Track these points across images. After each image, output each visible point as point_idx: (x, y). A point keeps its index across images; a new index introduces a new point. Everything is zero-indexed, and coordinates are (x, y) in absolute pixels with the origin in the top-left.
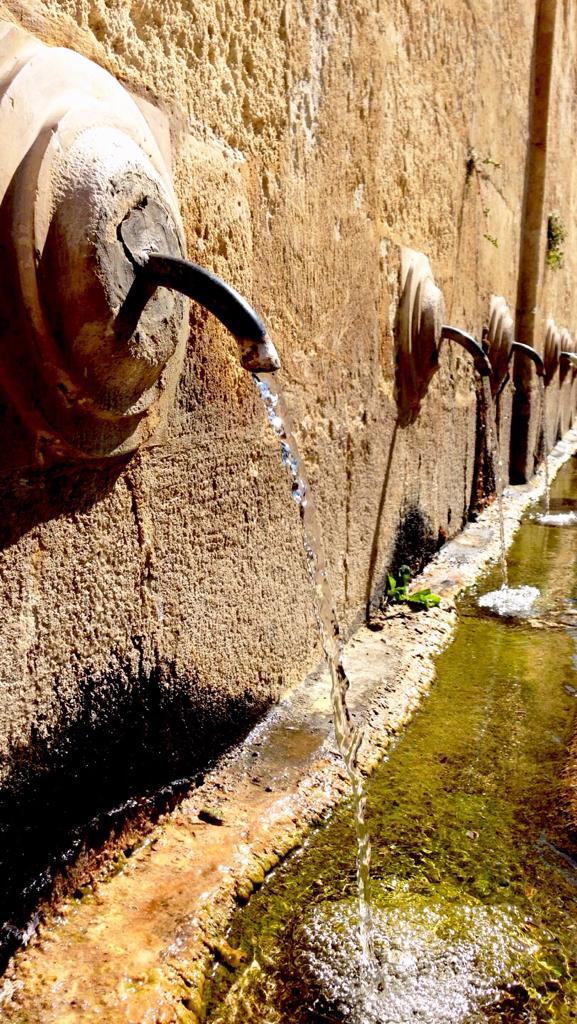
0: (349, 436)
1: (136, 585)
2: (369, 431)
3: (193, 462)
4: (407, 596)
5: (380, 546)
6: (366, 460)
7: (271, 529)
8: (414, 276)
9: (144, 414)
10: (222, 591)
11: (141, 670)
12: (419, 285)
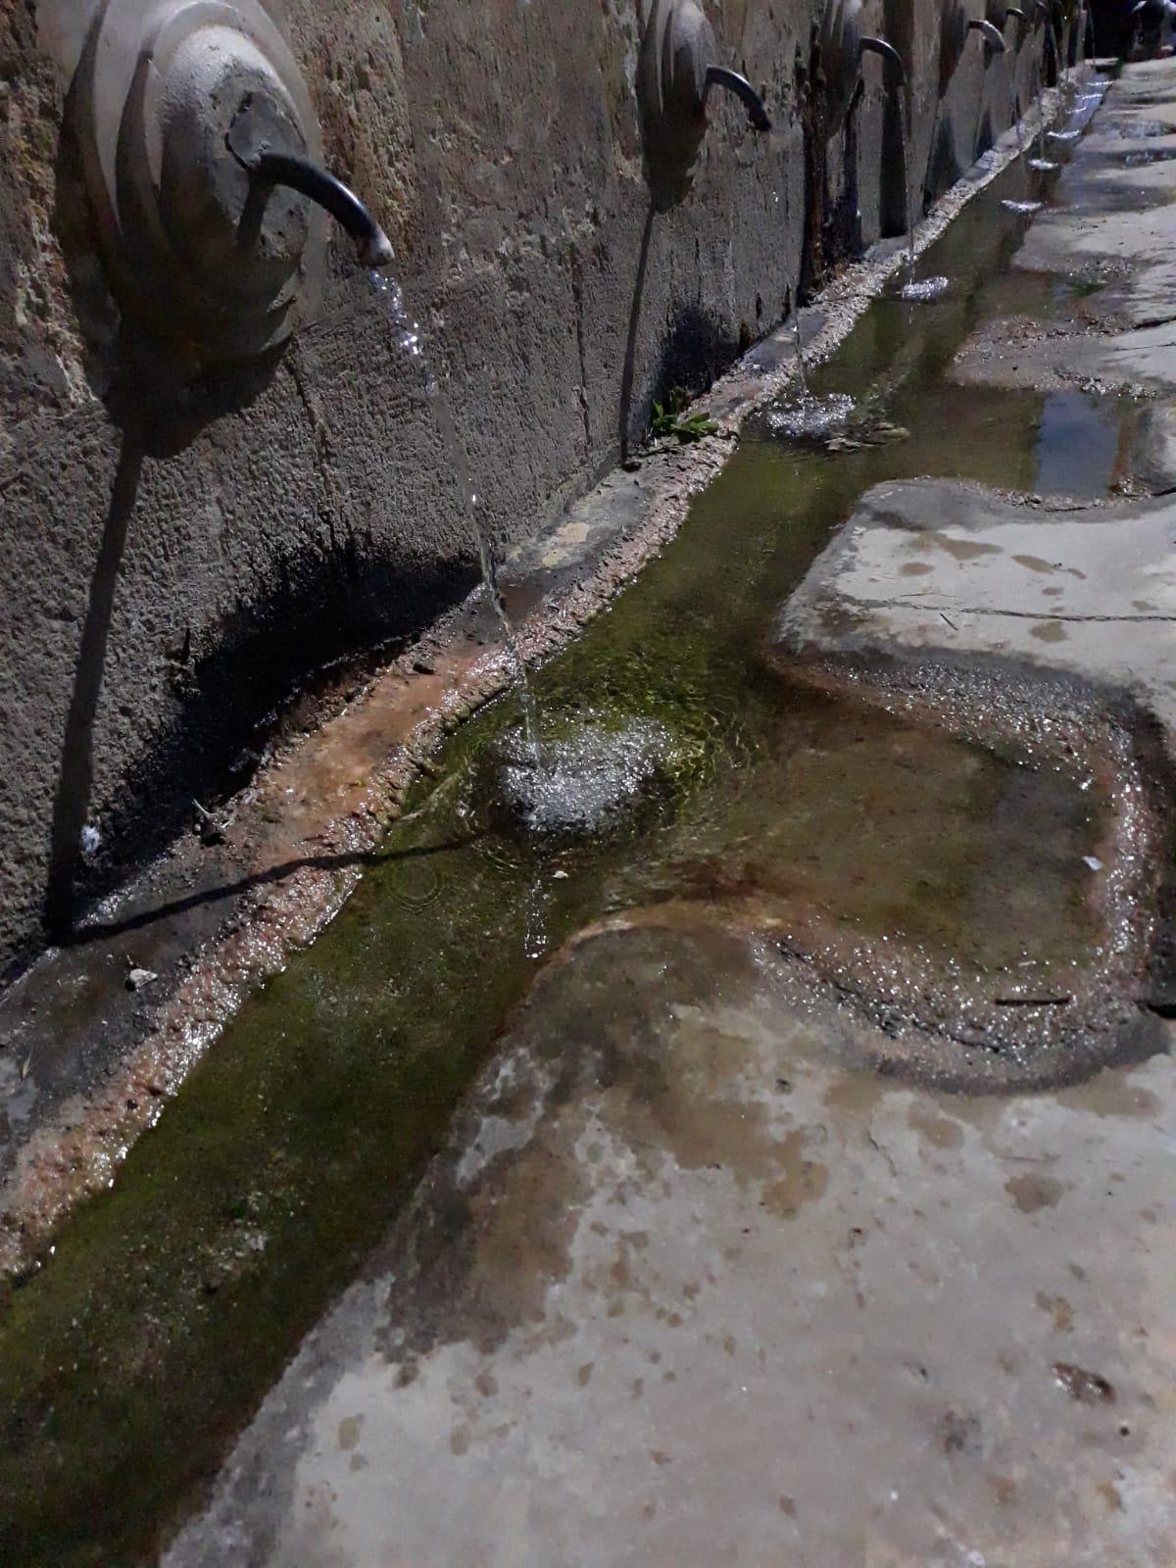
1: (315, 464)
3: (358, 329)
5: (637, 367)
6: (602, 270)
9: (291, 301)
11: (334, 543)
12: (670, 15)
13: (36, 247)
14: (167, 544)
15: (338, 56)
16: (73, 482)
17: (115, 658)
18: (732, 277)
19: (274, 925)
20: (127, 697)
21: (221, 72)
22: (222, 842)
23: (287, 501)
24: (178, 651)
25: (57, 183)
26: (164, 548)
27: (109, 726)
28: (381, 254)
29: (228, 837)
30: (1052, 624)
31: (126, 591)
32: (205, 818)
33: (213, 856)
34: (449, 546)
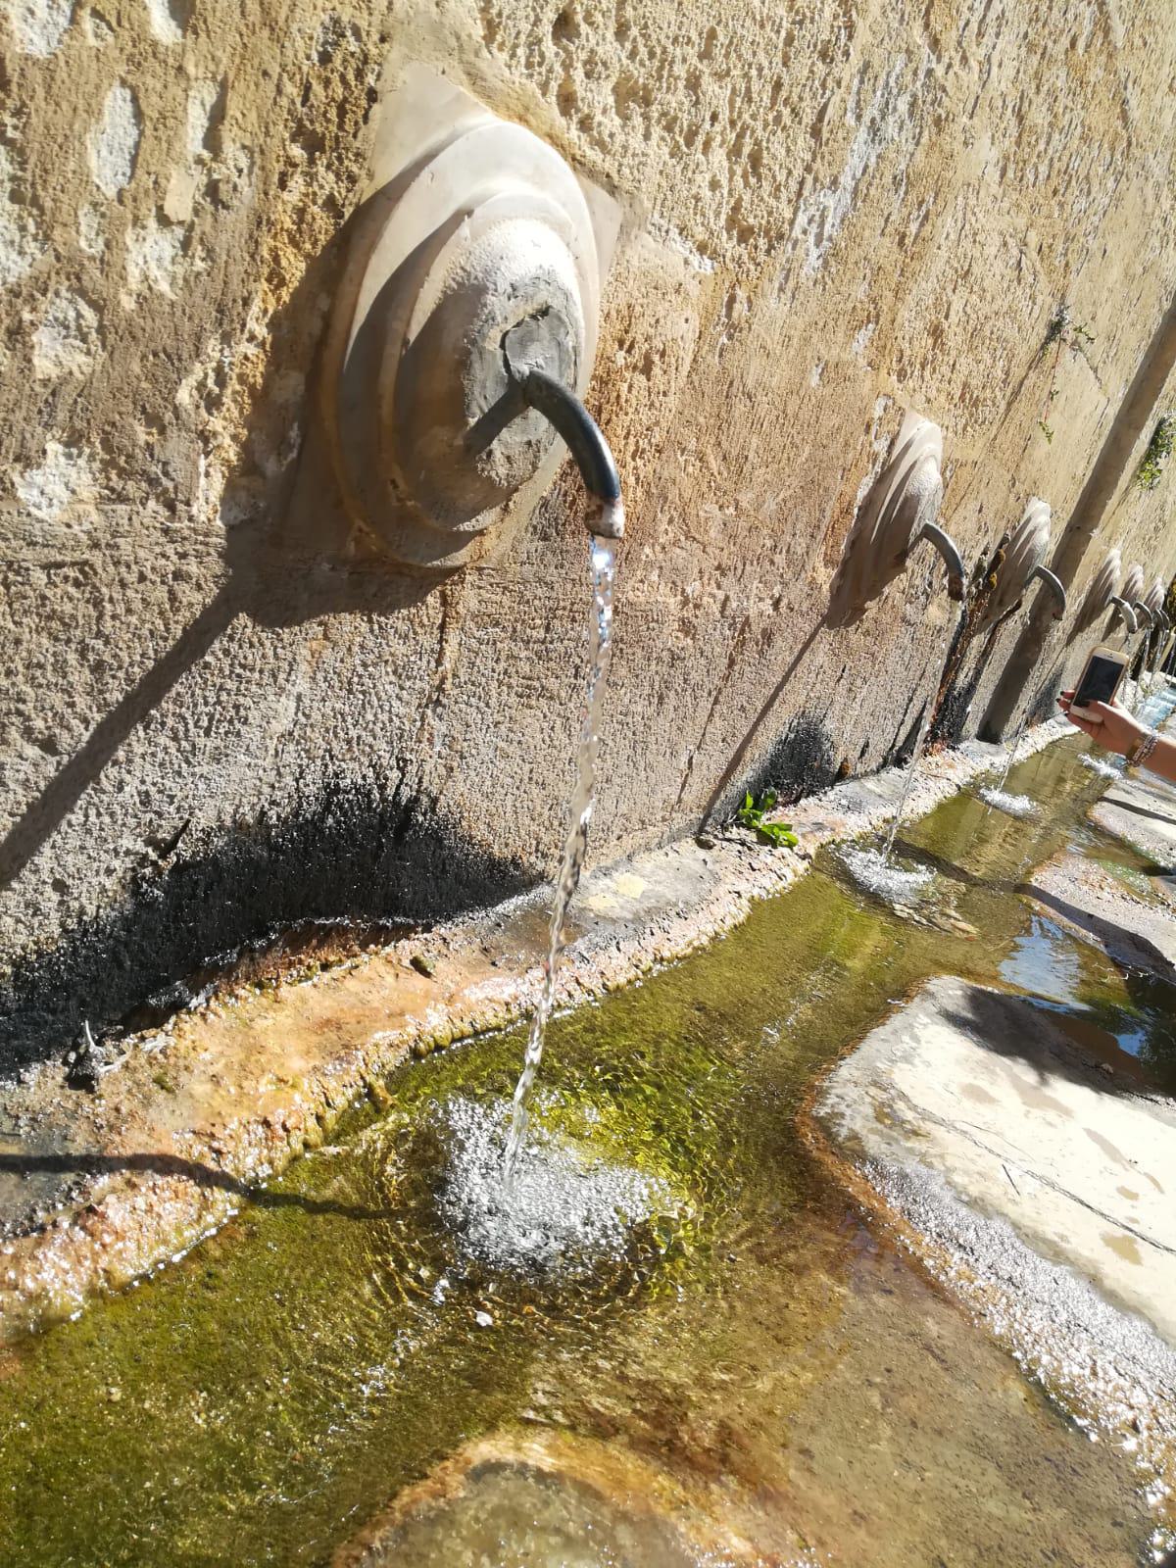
1: (420, 706)
2: (778, 620)
3: (528, 595)
5: (748, 755)
6: (761, 653)
9: (481, 533)
11: (397, 793)
12: (912, 467)
13: (242, 331)
14: (217, 716)
15: (640, 330)
16: (143, 600)
17: (83, 819)
19: (94, 1241)
20: (72, 870)
21: (533, 270)
22: (91, 1090)
23: (372, 731)
24: (164, 840)
25: (303, 281)
26: (210, 721)
27: (28, 896)
28: (612, 525)
29: (102, 1087)
30: (1125, 1237)
31: (139, 749)
32: (87, 1051)
33: (70, 1105)
34: (507, 845)
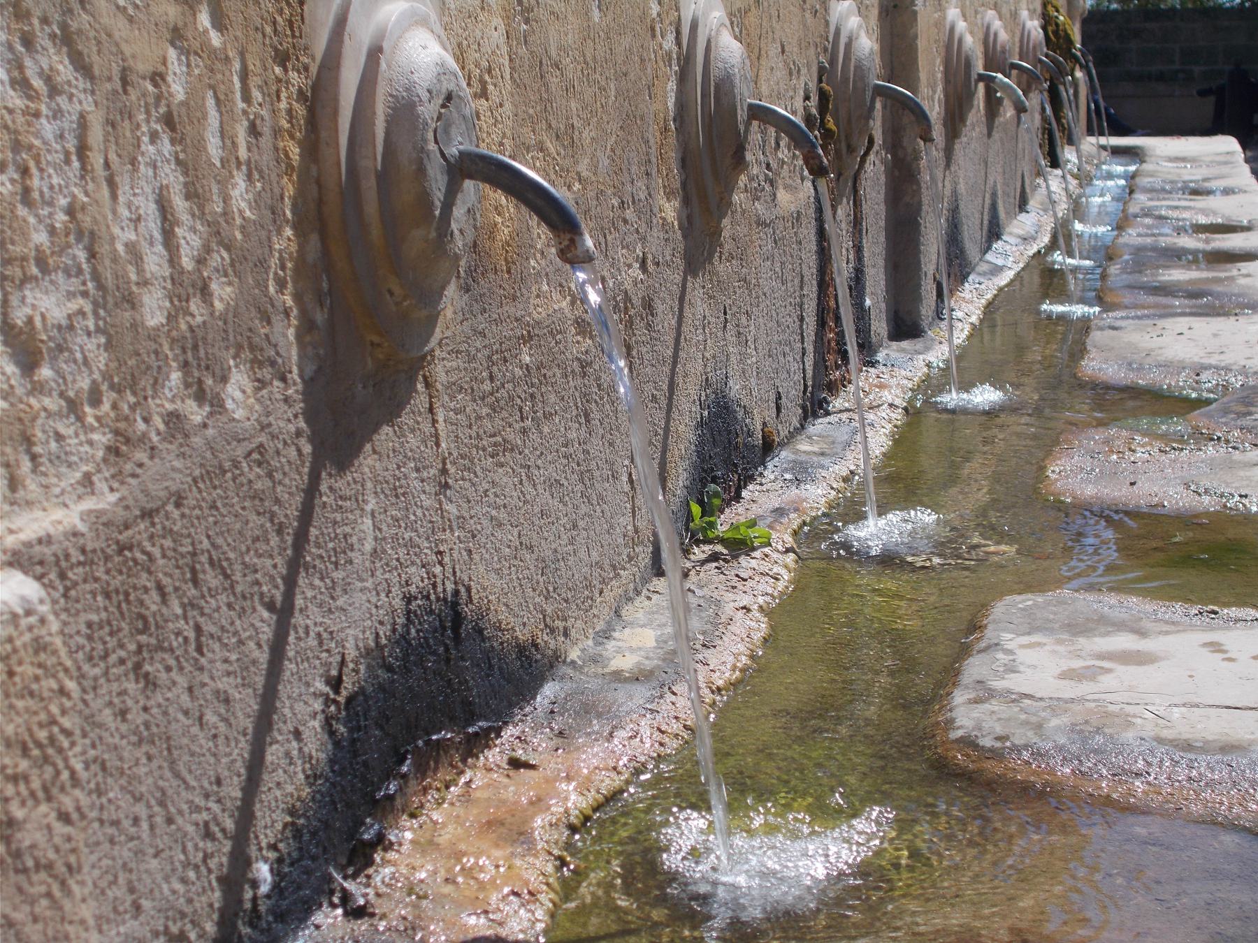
0: (626, 292)
1: (436, 494)
2: (651, 282)
4: (722, 528)
6: (649, 326)
7: (546, 430)
8: (700, 30)
10: (505, 506)
12: (709, 41)
18: (754, 359)
